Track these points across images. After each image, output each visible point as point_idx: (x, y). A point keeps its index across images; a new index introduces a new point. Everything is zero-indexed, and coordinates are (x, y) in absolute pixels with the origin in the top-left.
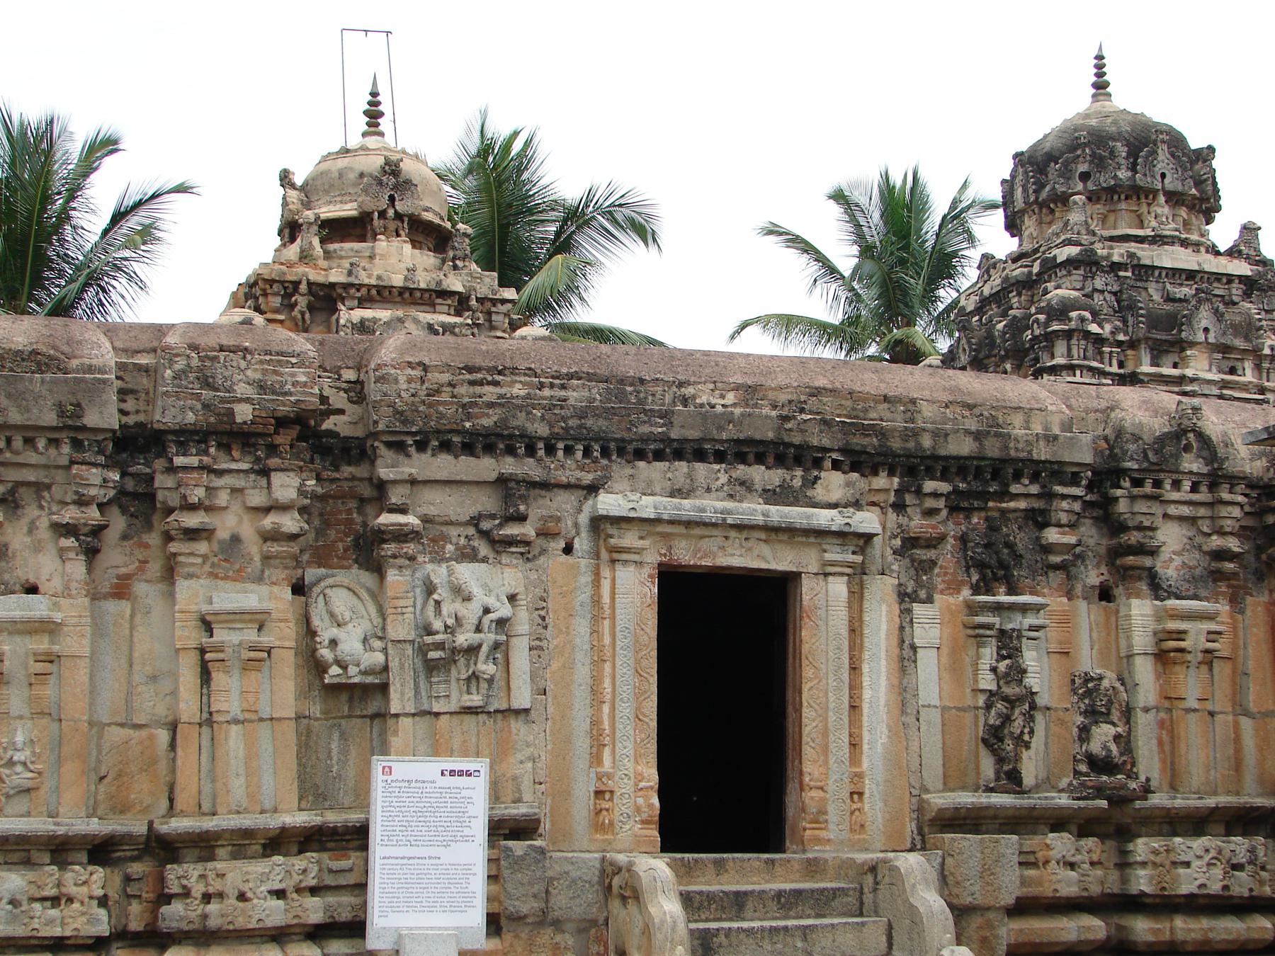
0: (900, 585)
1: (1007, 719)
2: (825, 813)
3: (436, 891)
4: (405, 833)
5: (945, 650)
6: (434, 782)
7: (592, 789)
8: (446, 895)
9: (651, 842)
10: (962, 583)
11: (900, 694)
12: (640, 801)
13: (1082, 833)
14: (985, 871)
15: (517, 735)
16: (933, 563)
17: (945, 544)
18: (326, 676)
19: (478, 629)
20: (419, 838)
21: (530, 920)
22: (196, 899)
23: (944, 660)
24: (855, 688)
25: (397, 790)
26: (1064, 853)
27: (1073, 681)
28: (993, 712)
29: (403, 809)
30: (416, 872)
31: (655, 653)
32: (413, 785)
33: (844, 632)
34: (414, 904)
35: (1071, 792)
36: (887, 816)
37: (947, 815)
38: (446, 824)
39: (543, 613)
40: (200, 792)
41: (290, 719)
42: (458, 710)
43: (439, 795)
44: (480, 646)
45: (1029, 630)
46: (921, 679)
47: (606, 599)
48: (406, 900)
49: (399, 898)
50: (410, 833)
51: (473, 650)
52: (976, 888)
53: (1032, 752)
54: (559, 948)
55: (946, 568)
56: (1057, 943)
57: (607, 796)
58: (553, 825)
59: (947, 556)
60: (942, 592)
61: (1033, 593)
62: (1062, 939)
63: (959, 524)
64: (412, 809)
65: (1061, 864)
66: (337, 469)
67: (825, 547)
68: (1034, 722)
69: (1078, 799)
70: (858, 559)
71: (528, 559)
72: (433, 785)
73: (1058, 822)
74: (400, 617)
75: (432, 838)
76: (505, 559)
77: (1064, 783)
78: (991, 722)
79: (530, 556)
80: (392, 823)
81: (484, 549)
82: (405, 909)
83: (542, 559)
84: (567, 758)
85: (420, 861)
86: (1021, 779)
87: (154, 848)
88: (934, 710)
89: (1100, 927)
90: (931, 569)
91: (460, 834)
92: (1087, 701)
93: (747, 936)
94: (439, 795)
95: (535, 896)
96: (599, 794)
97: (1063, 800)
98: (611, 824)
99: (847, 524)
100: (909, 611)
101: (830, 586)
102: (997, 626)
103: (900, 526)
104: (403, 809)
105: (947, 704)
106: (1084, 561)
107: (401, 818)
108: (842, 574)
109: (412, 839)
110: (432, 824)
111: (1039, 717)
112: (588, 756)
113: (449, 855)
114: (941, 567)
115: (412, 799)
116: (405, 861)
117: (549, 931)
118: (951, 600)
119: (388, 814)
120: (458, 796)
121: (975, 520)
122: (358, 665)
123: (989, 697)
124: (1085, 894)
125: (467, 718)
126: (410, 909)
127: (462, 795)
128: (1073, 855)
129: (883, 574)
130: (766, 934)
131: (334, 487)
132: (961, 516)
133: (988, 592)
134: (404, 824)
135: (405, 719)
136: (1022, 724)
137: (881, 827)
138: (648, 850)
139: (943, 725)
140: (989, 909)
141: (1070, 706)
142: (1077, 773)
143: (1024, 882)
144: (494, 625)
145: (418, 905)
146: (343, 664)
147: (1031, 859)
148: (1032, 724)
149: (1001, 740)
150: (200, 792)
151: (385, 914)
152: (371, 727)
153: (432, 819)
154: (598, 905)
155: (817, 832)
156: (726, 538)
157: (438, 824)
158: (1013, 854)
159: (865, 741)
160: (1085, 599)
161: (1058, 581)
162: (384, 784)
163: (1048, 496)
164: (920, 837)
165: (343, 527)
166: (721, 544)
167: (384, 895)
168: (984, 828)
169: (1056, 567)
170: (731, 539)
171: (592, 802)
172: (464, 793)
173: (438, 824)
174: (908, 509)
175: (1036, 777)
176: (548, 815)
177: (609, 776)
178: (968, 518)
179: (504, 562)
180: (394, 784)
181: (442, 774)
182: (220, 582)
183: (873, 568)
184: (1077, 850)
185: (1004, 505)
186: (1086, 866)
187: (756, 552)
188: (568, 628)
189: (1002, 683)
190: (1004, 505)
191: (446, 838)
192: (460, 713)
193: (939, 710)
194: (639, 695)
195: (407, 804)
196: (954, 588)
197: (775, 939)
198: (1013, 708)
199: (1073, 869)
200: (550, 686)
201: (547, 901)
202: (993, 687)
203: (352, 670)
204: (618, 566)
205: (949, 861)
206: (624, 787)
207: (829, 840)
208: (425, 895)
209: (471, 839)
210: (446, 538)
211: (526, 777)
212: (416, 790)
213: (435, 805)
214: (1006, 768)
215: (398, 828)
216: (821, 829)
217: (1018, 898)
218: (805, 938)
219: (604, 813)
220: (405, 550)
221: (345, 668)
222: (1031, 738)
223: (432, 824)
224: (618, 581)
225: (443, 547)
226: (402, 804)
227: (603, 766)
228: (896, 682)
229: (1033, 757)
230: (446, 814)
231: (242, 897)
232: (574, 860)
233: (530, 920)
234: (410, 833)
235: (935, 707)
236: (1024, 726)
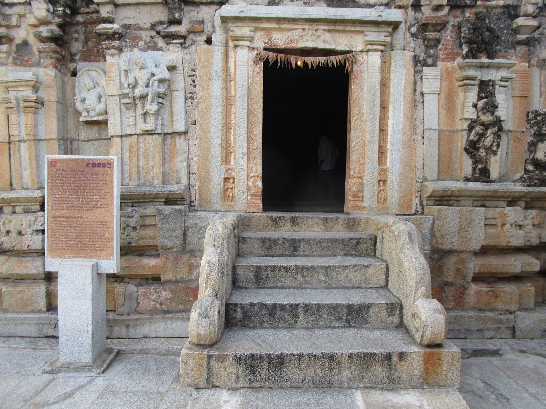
0: (415, 56)
1: (482, 136)
2: (363, 192)
5: (443, 96)
7: (222, 177)
9: (256, 207)
10: (457, 54)
11: (411, 122)
12: (250, 183)
13: (527, 207)
14: (461, 229)
15: (179, 146)
16: (438, 41)
17: (446, 31)
18: (81, 117)
19: (147, 86)
21: (175, 250)
23: (442, 102)
24: (383, 119)
26: (516, 219)
27: (528, 115)
28: (474, 132)
31: (261, 101)
33: (378, 85)
35: (524, 182)
36: (401, 194)
37: (438, 194)
39: (194, 78)
40: (11, 179)
41: (55, 139)
42: (141, 133)
44: (147, 95)
45: (501, 81)
46: (426, 112)
47: (232, 69)
52: (454, 240)
53: (497, 157)
55: (446, 45)
56: (507, 273)
57: (231, 181)
58: (200, 197)
59: (448, 35)
60: (443, 60)
61: (504, 57)
62: (510, 271)
63: (455, 17)
65: (514, 226)
66: (88, 7)
67: (366, 33)
68: (500, 139)
69: (529, 186)
70: (389, 39)
71: (185, 47)
73: (512, 201)
74: (112, 82)
76: (171, 47)
77: (518, 176)
78: (471, 138)
79: (186, 45)
81: (161, 43)
83: (193, 47)
86: (489, 173)
88: (434, 131)
89: (536, 264)
90: (436, 46)
92: (535, 128)
93: (287, 271)
95: (177, 237)
97: (519, 188)
98: (233, 196)
99: (380, 16)
100: (421, 72)
101: (369, 57)
102: (479, 78)
103: (416, 19)
105: (443, 128)
106: (539, 43)
108: (377, 50)
111: (504, 136)
112: (220, 159)
114: (443, 45)
116: (65, 219)
117: (187, 256)
118: (449, 64)
121: (467, 14)
122: (95, 110)
123: (471, 123)
124: (528, 244)
125: (147, 137)
128: (522, 220)
129: (404, 50)
130: (300, 270)
131: (89, 17)
132: (458, 12)
133: (474, 57)
135: (117, 139)
136: (492, 139)
137: (397, 200)
139: (439, 141)
140: (462, 252)
141: (525, 130)
142: (527, 171)
143: (487, 236)
146: (88, 110)
147: (493, 222)
148: (499, 140)
149: (477, 149)
150: (11, 179)
155: (357, 203)
156: (304, 29)
158: (481, 219)
159: (389, 151)
160: (538, 67)
161: (522, 52)
164: (421, 207)
165: (96, 40)
166: (300, 34)
168: (462, 203)
169: (519, 43)
170: (307, 30)
171: (222, 184)
174: (423, 8)
175: (499, 173)
176: (197, 191)
177: (233, 170)
178: (463, 12)
179: (170, 49)
181: (88, 166)
182: (18, 67)
183: (399, 46)
184: (525, 217)
185: (488, 3)
186: (530, 227)
187: (322, 38)
188: (208, 86)
189: (480, 114)
190: (488, 3)
192: (143, 134)
193: (437, 132)
194: (250, 124)
196: (451, 57)
197: (305, 274)
198: (487, 129)
199: (520, 229)
200: (198, 120)
202: (474, 117)
203: (92, 114)
204: (238, 49)
205: (437, 222)
206: (241, 176)
207: (364, 207)
210: (139, 38)
211: (183, 170)
214: (480, 166)
216: (360, 201)
217: (482, 246)
218: (326, 274)
219: (230, 190)
220: (113, 44)
221: (88, 112)
222: (497, 149)
224: (238, 58)
225: (138, 43)
227: (230, 164)
228: (409, 115)
229: (498, 160)
231: (20, 233)
232: (201, 217)
233: (175, 250)
235: (435, 130)
236: (494, 141)
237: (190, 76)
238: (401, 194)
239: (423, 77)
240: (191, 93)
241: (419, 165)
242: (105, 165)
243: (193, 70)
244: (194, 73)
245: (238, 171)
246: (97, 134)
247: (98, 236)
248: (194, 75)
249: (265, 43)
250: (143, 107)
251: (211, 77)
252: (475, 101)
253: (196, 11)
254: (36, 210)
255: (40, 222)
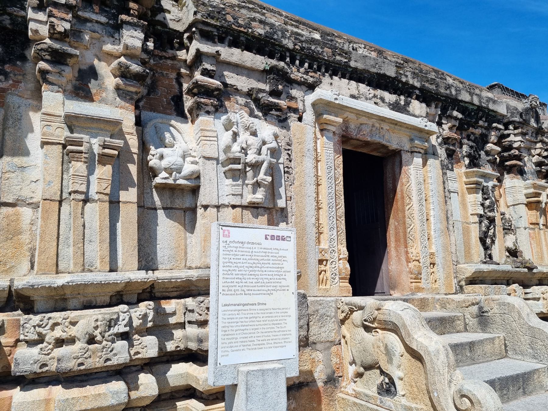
3: (264, 331)
4: (241, 284)
6: (259, 244)
8: (270, 334)
20: (251, 288)
22: (50, 344)
25: (234, 249)
29: (239, 265)
30: (248, 316)
32: (246, 245)
34: (249, 343)
38: (269, 277)
43: (264, 254)
48: (242, 340)
49: (236, 339)
50: (244, 284)
51: (256, 166)
54: (314, 362)
57: (324, 263)
64: (245, 265)
72: (260, 246)
75: (260, 288)
80: (230, 276)
82: (242, 348)
84: (304, 238)
85: (252, 307)
87: (15, 300)
88: (459, 223)
91: (278, 284)
94: (264, 254)
96: (321, 262)
100: (446, 174)
104: (239, 265)
107: (237, 272)
109: (245, 289)
110: (260, 277)
113: (273, 301)
115: (245, 257)
119: (227, 269)
120: (277, 255)
126: (245, 348)
127: (280, 255)
134: (240, 277)
138: (345, 295)
144: (269, 151)
145: (251, 343)
151: (226, 353)
152: (185, 216)
153: (259, 273)
154: (334, 331)
157: (264, 277)
162: (224, 244)
163: (489, 128)
167: (226, 337)
172: (281, 253)
173: (264, 277)
180: (231, 245)
181: (266, 238)
191: (270, 288)
195: (241, 261)
201: (308, 332)
208: (256, 335)
209: (286, 288)
212: (248, 250)
213: (261, 262)
215: (236, 280)
223: (260, 277)
226: (238, 261)
230: (269, 269)
234: (244, 284)
237: (286, 150)
238: (445, 275)
239: (448, 178)
240: (287, 167)
241: (453, 250)
242: (285, 238)
243: (289, 145)
244: (290, 148)
245: (331, 253)
246: (169, 202)
247: (279, 328)
248: (289, 150)
249: (343, 131)
250: (255, 176)
251: (304, 154)
252: (481, 200)
253: (290, 87)
254: (104, 303)
255: (124, 320)
